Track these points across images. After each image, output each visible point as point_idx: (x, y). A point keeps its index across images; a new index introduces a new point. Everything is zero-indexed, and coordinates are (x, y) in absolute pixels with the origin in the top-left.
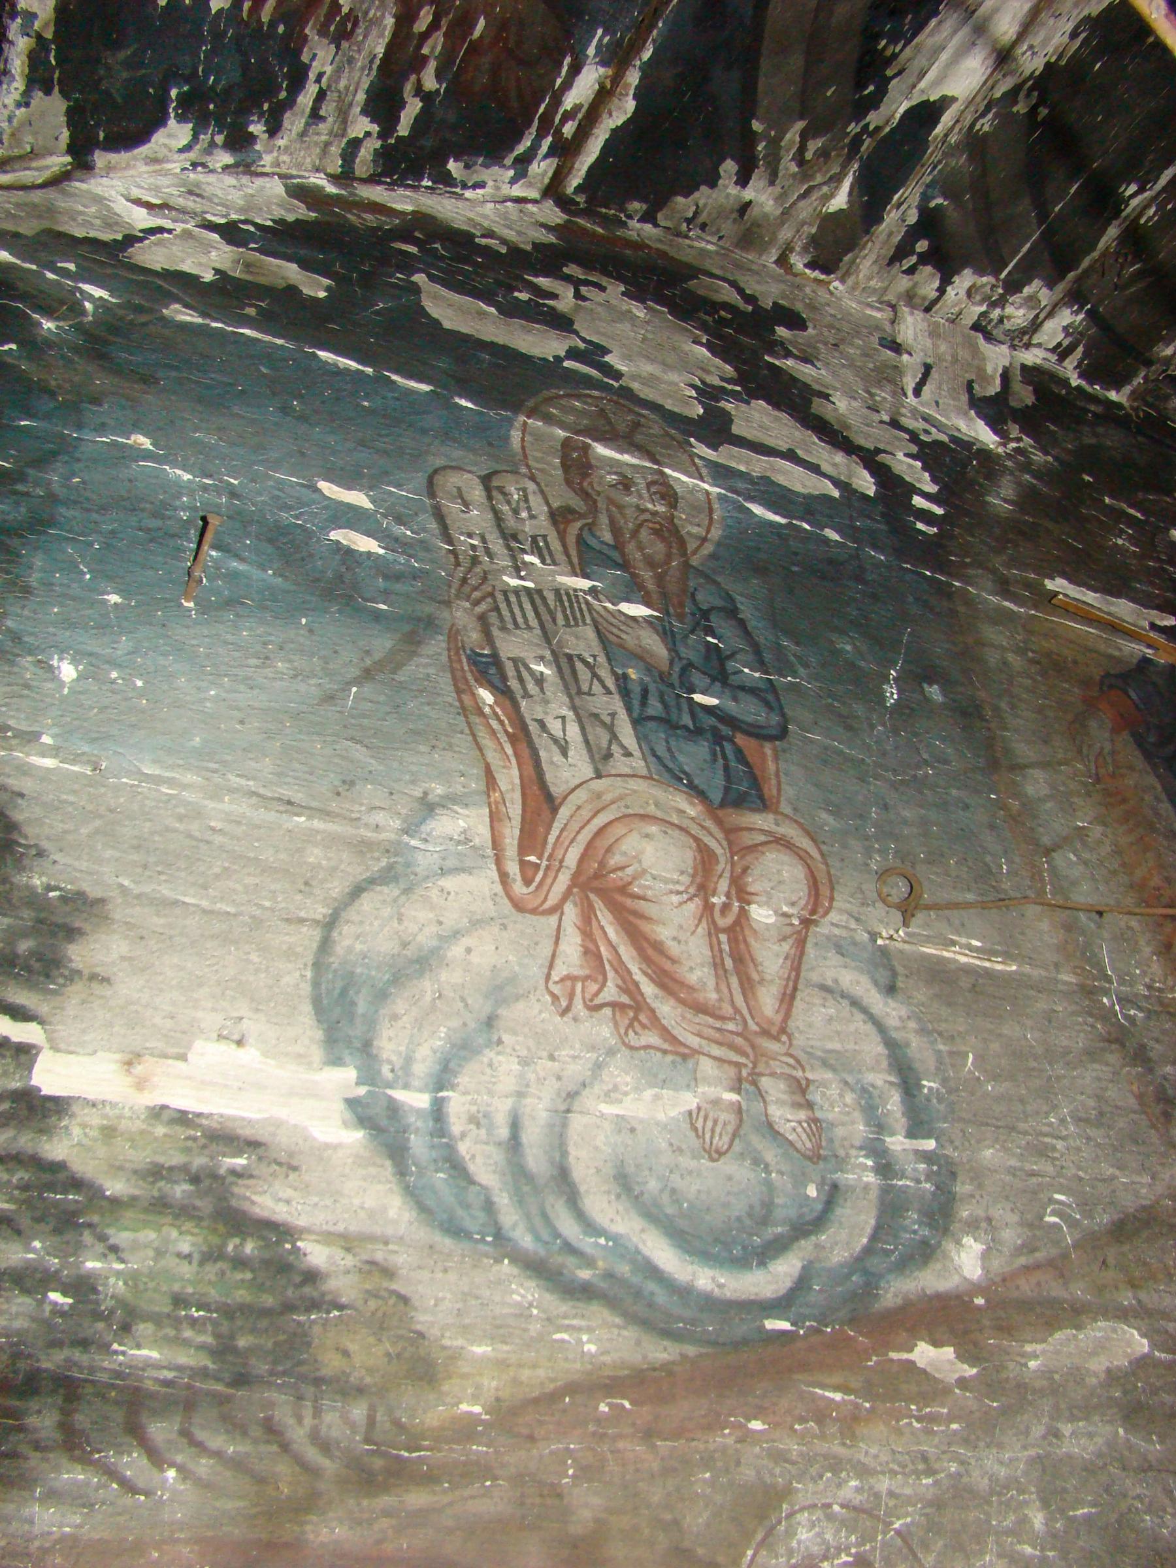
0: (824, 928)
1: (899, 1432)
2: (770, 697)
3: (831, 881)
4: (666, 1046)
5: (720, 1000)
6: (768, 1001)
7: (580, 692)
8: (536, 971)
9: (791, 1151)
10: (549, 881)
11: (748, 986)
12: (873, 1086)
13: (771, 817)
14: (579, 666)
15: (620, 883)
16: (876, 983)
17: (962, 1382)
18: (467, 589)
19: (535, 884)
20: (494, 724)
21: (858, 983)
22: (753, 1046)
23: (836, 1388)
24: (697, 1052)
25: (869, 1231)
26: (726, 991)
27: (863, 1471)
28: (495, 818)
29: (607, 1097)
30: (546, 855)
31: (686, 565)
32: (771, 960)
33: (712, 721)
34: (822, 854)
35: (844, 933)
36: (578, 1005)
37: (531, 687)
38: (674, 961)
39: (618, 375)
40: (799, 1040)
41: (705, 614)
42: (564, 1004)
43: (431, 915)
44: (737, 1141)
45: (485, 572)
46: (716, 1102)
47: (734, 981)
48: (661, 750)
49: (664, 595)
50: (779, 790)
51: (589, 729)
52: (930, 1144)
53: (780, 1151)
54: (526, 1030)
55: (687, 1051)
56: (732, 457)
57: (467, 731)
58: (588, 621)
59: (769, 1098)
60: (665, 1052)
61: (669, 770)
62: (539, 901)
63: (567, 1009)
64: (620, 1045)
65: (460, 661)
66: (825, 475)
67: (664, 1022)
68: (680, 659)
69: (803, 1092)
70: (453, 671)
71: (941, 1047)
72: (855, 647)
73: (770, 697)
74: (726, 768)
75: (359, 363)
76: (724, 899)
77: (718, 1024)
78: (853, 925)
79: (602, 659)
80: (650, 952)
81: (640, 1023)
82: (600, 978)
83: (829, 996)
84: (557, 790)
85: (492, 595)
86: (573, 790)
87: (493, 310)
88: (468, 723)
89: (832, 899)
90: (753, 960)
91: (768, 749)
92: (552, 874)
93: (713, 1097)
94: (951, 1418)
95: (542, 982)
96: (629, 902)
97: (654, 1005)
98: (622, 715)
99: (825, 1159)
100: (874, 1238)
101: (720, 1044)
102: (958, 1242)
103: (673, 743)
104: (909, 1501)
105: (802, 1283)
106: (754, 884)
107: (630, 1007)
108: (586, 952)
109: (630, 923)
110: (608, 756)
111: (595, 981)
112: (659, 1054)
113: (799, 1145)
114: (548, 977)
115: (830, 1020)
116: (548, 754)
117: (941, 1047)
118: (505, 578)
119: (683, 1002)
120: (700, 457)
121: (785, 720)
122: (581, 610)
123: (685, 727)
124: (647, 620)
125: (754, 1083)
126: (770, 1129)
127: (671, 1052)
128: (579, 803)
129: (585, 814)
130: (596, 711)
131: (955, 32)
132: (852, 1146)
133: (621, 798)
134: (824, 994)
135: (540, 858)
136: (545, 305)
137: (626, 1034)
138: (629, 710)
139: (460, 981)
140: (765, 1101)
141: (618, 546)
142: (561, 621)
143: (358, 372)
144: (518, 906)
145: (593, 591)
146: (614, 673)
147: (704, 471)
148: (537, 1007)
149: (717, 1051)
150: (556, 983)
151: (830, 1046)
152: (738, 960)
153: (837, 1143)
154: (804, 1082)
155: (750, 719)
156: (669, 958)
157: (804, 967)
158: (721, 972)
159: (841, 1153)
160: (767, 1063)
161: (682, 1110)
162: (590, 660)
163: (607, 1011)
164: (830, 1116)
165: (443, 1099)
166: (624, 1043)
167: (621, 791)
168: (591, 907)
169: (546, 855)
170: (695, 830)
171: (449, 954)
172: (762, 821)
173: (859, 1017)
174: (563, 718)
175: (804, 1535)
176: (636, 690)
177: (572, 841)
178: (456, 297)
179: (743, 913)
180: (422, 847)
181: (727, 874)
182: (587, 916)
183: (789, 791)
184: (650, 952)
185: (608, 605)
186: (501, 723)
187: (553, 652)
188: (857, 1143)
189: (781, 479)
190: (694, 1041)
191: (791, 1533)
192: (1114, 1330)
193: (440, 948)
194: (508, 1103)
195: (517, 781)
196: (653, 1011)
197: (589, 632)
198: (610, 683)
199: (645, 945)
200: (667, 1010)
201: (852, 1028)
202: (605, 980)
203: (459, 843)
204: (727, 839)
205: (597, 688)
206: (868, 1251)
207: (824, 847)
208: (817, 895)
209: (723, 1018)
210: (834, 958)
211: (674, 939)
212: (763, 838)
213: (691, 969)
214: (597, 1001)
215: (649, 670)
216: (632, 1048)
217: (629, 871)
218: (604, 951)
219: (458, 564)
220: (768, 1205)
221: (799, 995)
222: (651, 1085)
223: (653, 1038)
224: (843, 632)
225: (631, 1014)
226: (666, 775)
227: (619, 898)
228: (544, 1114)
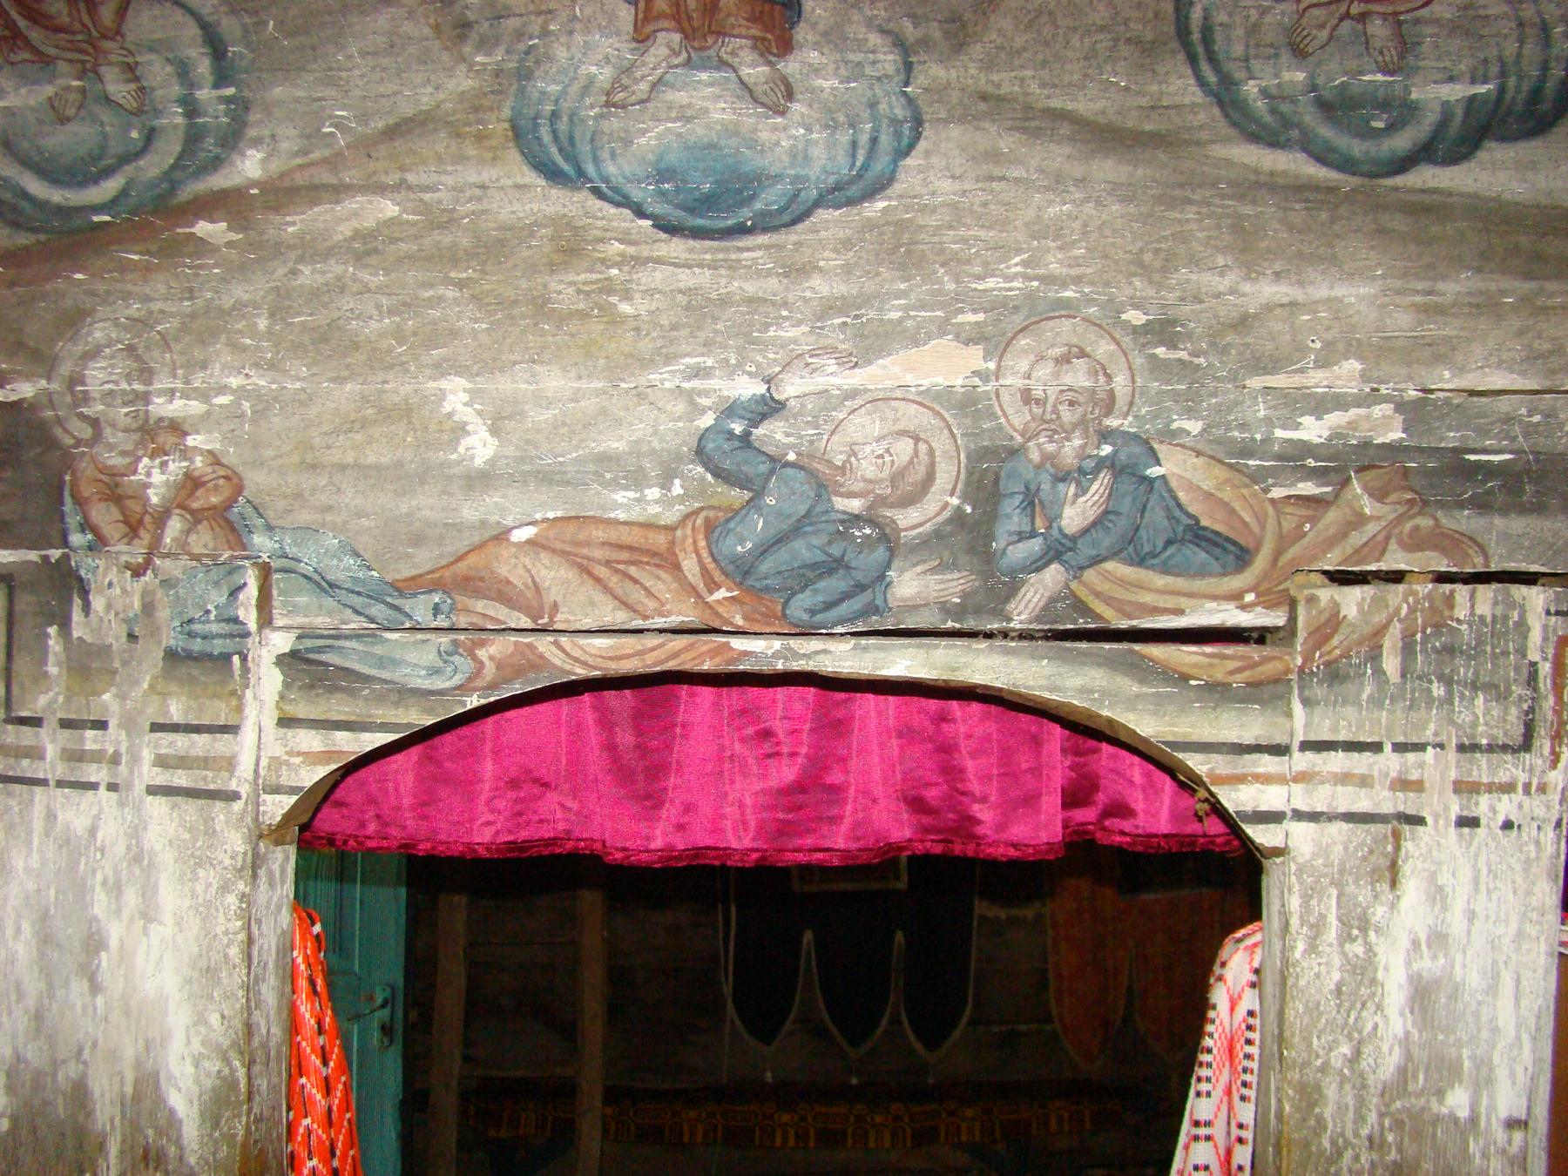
1: (177, 276)
17: (229, 244)
23: (135, 253)
24: (56, 58)
25: (175, 154)
27: (147, 299)
52: (231, 91)
71: (247, 20)
94: (215, 266)
100: (180, 158)
101: (70, 50)
102: (244, 155)
104: (172, 315)
105: (124, 192)
117: (247, 20)
119: (46, 28)
131: (1513, 98)
149: (69, 55)
175: (98, 334)
191: (89, 334)
192: (370, 202)
206: (174, 167)
209: (73, 33)
216: (12, 64)
220: (104, 147)
223: (27, 55)
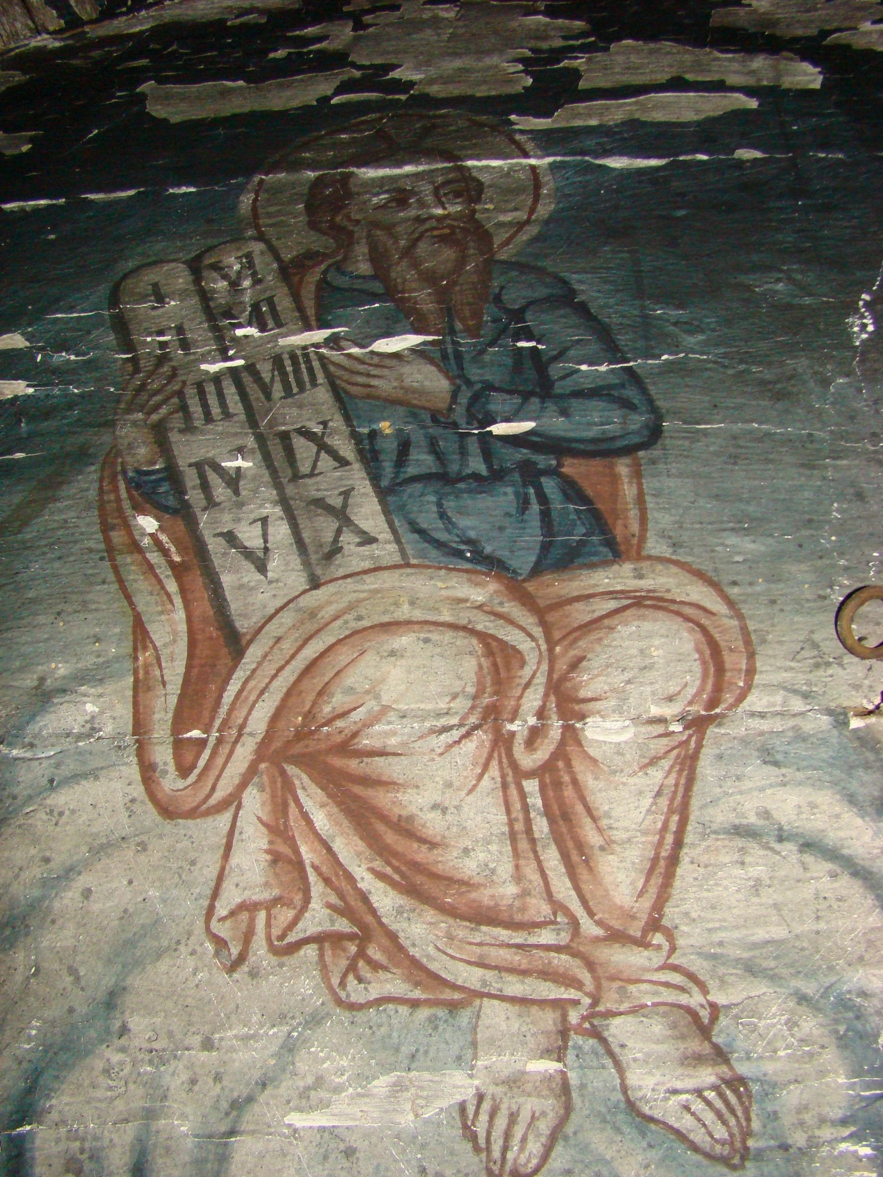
0: (738, 726)
2: (631, 393)
3: (748, 642)
4: (417, 994)
5: (525, 893)
6: (621, 877)
7: (296, 477)
8: (190, 908)
9: (680, 1149)
10: (220, 761)
11: (577, 858)
12: (863, 994)
13: (627, 567)
14: (299, 442)
15: (339, 739)
16: (851, 799)
18: (144, 396)
19: (197, 771)
20: (154, 557)
21: (813, 806)
22: (591, 966)
26: (536, 877)
28: (141, 688)
29: (305, 1100)
30: (217, 723)
31: (489, 265)
32: (626, 808)
33: (524, 453)
34: (730, 603)
35: (778, 725)
36: (259, 946)
37: (221, 492)
38: (433, 846)
39: (406, 86)
40: (690, 937)
41: (518, 315)
42: (235, 951)
43: (33, 851)
44: (559, 1149)
45: (174, 369)
46: (514, 1082)
47: (552, 857)
48: (428, 519)
49: (449, 312)
50: (643, 520)
51: (303, 523)
53: (654, 1155)
54: (169, 1004)
55: (457, 996)
56: (579, 115)
57: (111, 577)
58: (321, 378)
59: (626, 1057)
60: (415, 1004)
61: (439, 545)
62: (201, 796)
63: (242, 958)
64: (331, 1005)
65: (116, 490)
66: (733, 89)
67: (412, 951)
68: (469, 383)
69: (705, 1032)
70: (102, 507)
72: (790, 280)
73: (631, 393)
74: (546, 515)
75: (51, 199)
76: (532, 721)
77: (518, 938)
78: (797, 705)
79: (337, 422)
80: (390, 837)
81: (370, 962)
82: (298, 898)
83: (753, 847)
84: (243, 625)
85: (180, 394)
86: (271, 617)
87: (241, 83)
88: (116, 569)
89: (751, 671)
90: (589, 810)
91: (623, 467)
92: (224, 750)
93: (506, 1073)
95: (200, 924)
96: (353, 765)
97: (394, 927)
98: (363, 487)
99: (759, 1156)
101: (524, 973)
103: (450, 504)
106: (590, 682)
107: (351, 937)
108: (276, 858)
109: (356, 798)
110: (335, 550)
111: (289, 904)
112: (404, 1010)
113: (699, 1137)
114: (210, 911)
115: (757, 886)
116: (234, 576)
118: (204, 367)
119: (451, 912)
120: (522, 132)
121: (658, 415)
122: (310, 370)
123: (476, 476)
124: (416, 352)
125: (596, 1034)
126: (635, 1114)
127: (428, 1003)
128: (280, 632)
129: (288, 646)
130: (319, 495)
132: (822, 1121)
133: (350, 608)
134: (739, 842)
135: (207, 731)
136: (310, 52)
137: (343, 984)
138: (375, 478)
139: (70, 943)
140: (617, 1064)
141: (381, 272)
142: (277, 390)
143: (49, 206)
144: (168, 811)
145: (333, 342)
146: (355, 436)
147: (529, 146)
148: (191, 963)
149: (515, 987)
150: (222, 919)
151: (761, 934)
152: (561, 818)
153: (787, 1120)
154: (704, 1014)
155: (593, 432)
156: (423, 841)
157: (695, 803)
158: (523, 845)
159: (799, 1139)
160: (622, 991)
161: (444, 1104)
162: (317, 429)
163: (310, 952)
164: (769, 1067)
165: (22, 1137)
166: (339, 1002)
167: (353, 597)
168: (288, 786)
169: (217, 723)
170: (483, 624)
171: (57, 904)
172: (618, 577)
173: (821, 867)
174: (264, 521)
176: (390, 447)
177: (262, 693)
178: (195, 88)
179: (571, 735)
180: (29, 755)
181: (541, 679)
182: (283, 798)
183: (661, 519)
184: (390, 837)
185: (355, 350)
186: (165, 552)
187: (261, 439)
188: (837, 1114)
189: (659, 116)
190: (472, 977)
193: (43, 898)
194: (130, 1131)
195: (183, 627)
196: (393, 936)
197: (322, 395)
198: (347, 450)
199: (381, 828)
200: (420, 931)
201: (807, 891)
202: (307, 900)
203: (80, 737)
204: (543, 623)
205: (326, 462)
207: (734, 591)
208: (720, 670)
210: (758, 773)
211: (435, 807)
212: (612, 605)
213: (466, 851)
214: (291, 938)
215: (415, 415)
216: (353, 1007)
217: (355, 716)
218: (308, 853)
219: (137, 370)
221: (686, 854)
222: (386, 1068)
223: (393, 984)
224: (768, 268)
225: (353, 949)
226: (434, 553)
227: (337, 762)
228: (190, 1143)
